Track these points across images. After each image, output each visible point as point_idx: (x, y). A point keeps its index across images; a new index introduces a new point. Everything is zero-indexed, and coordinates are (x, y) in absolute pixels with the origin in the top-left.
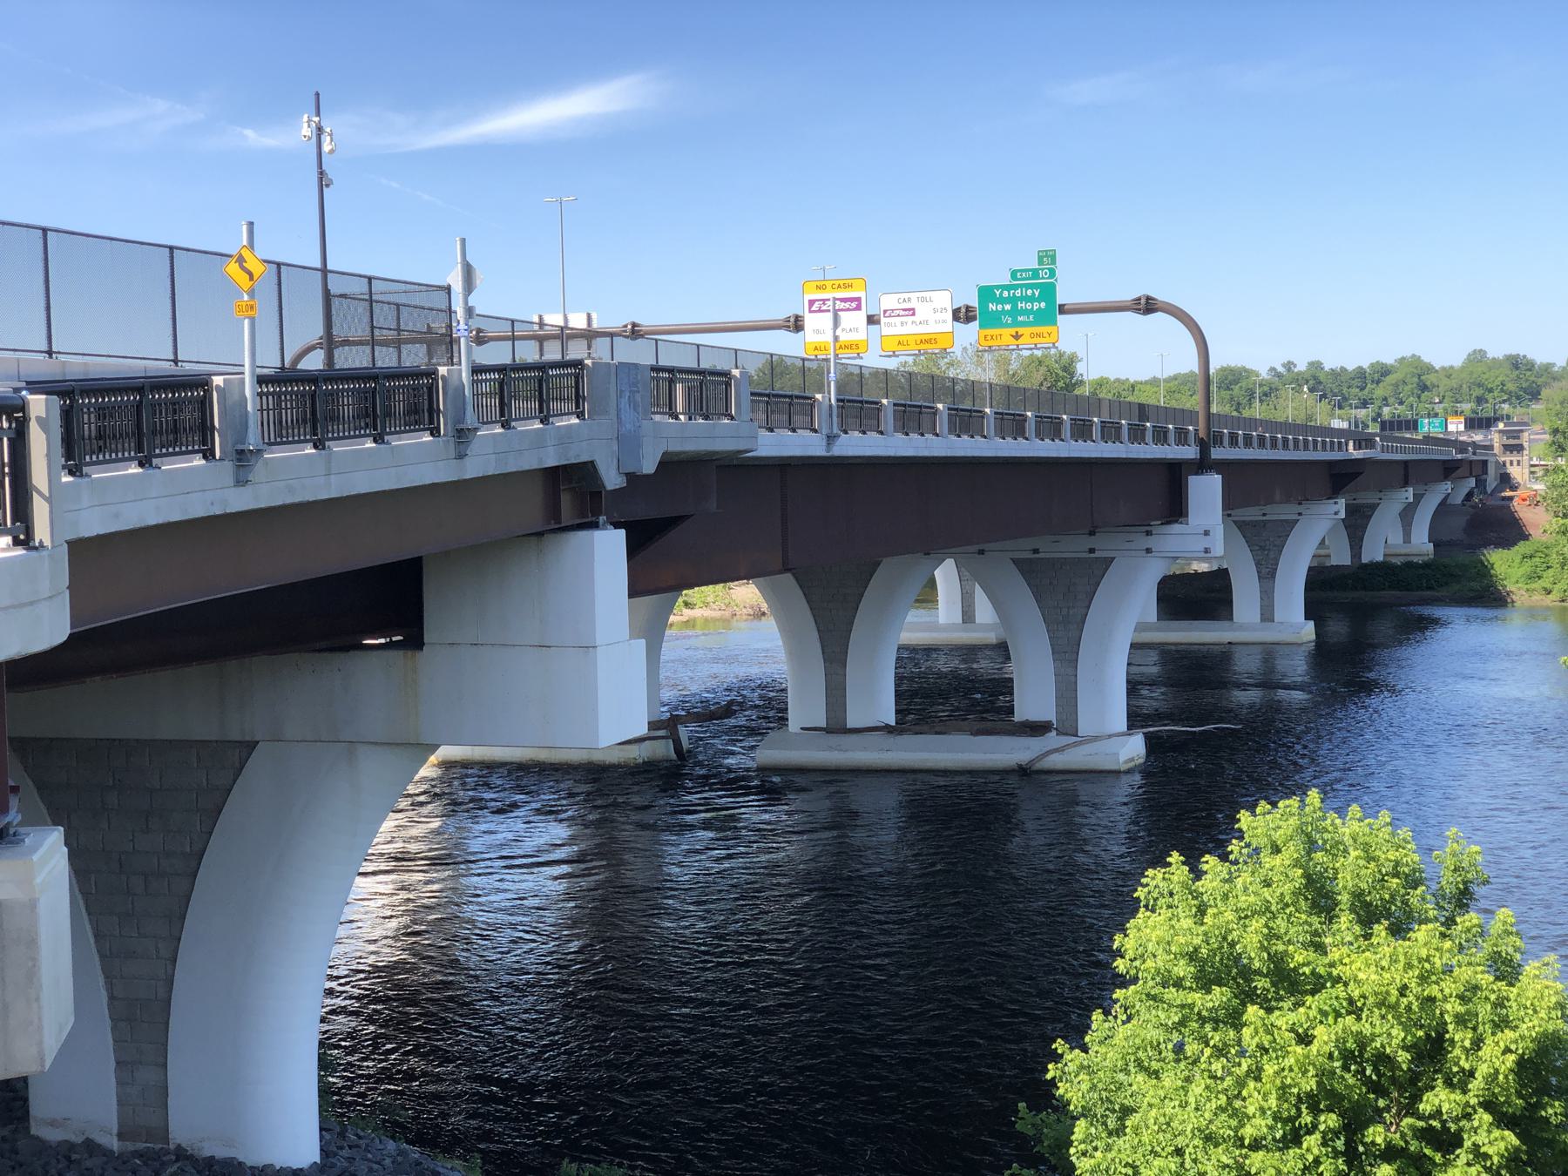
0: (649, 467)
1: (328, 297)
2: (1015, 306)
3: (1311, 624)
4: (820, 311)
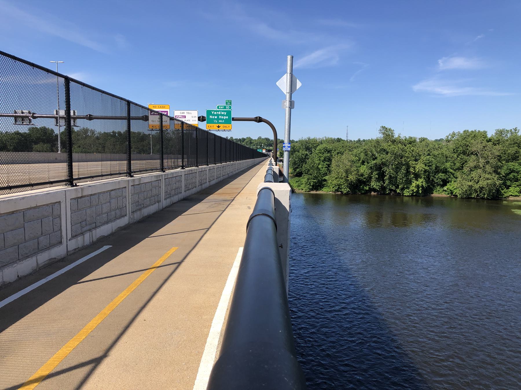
2: (218, 117)
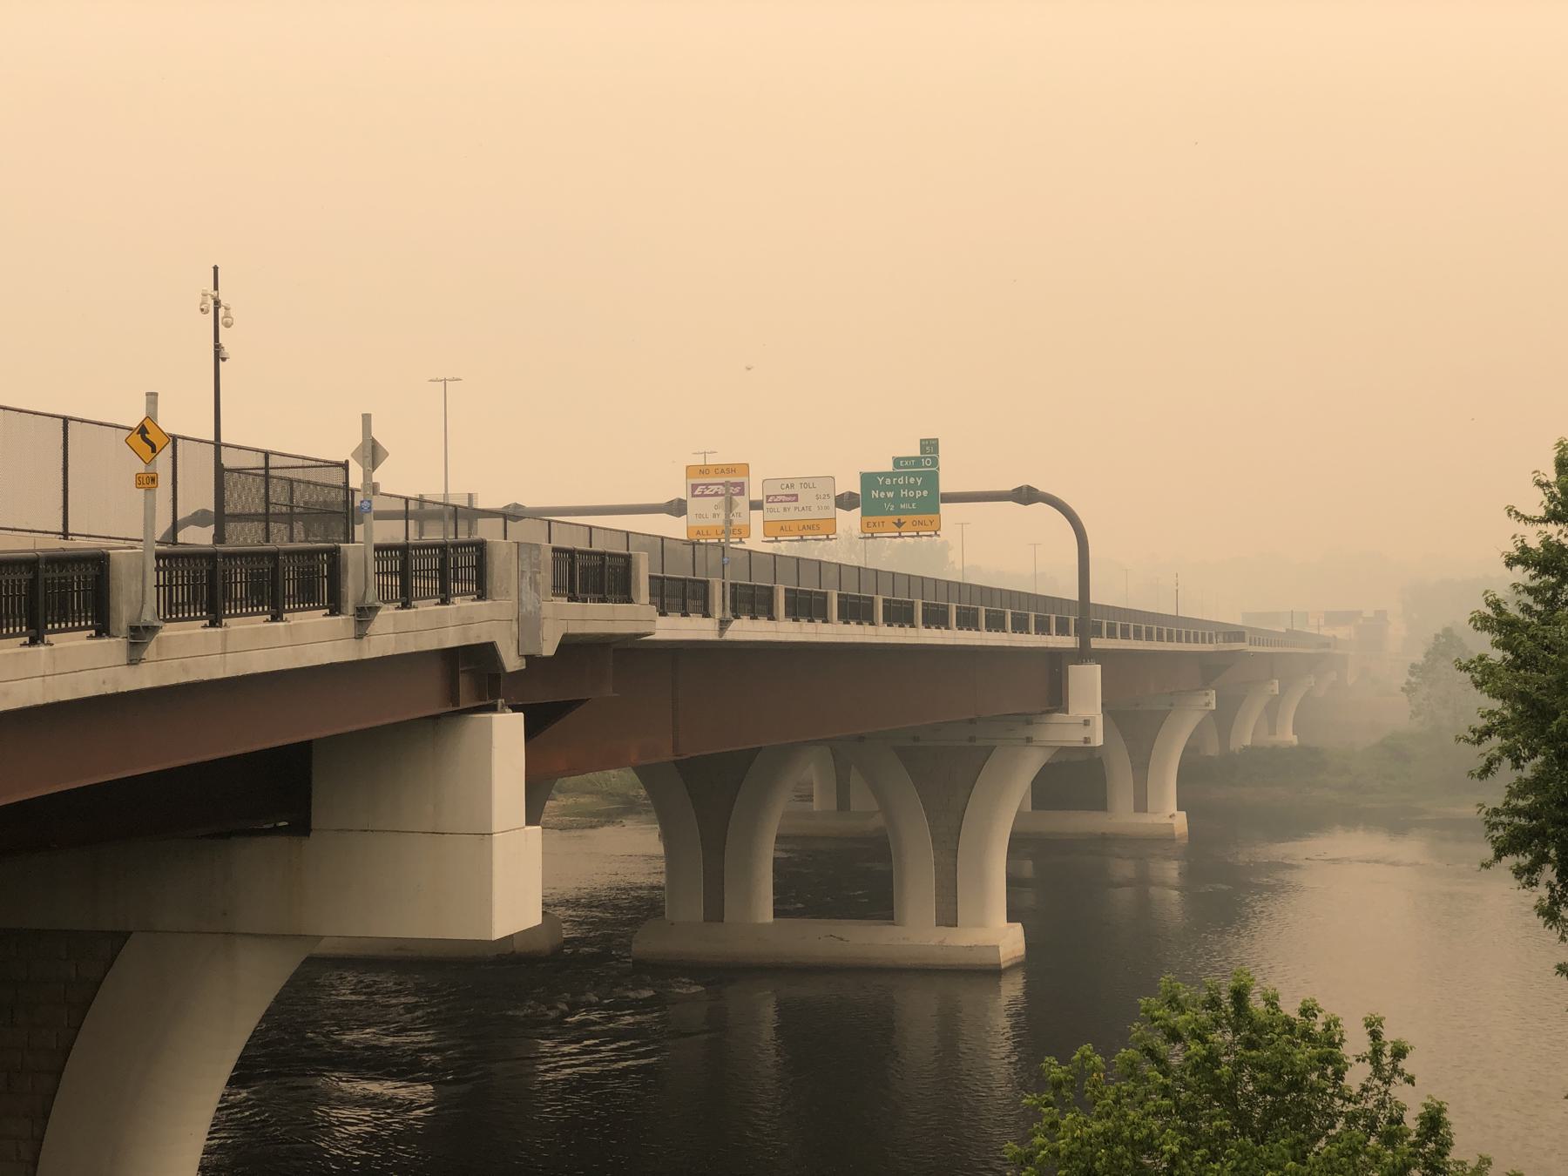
0: (549, 650)
1: (220, 470)
2: (897, 494)
3: (1018, 928)
4: (703, 495)
